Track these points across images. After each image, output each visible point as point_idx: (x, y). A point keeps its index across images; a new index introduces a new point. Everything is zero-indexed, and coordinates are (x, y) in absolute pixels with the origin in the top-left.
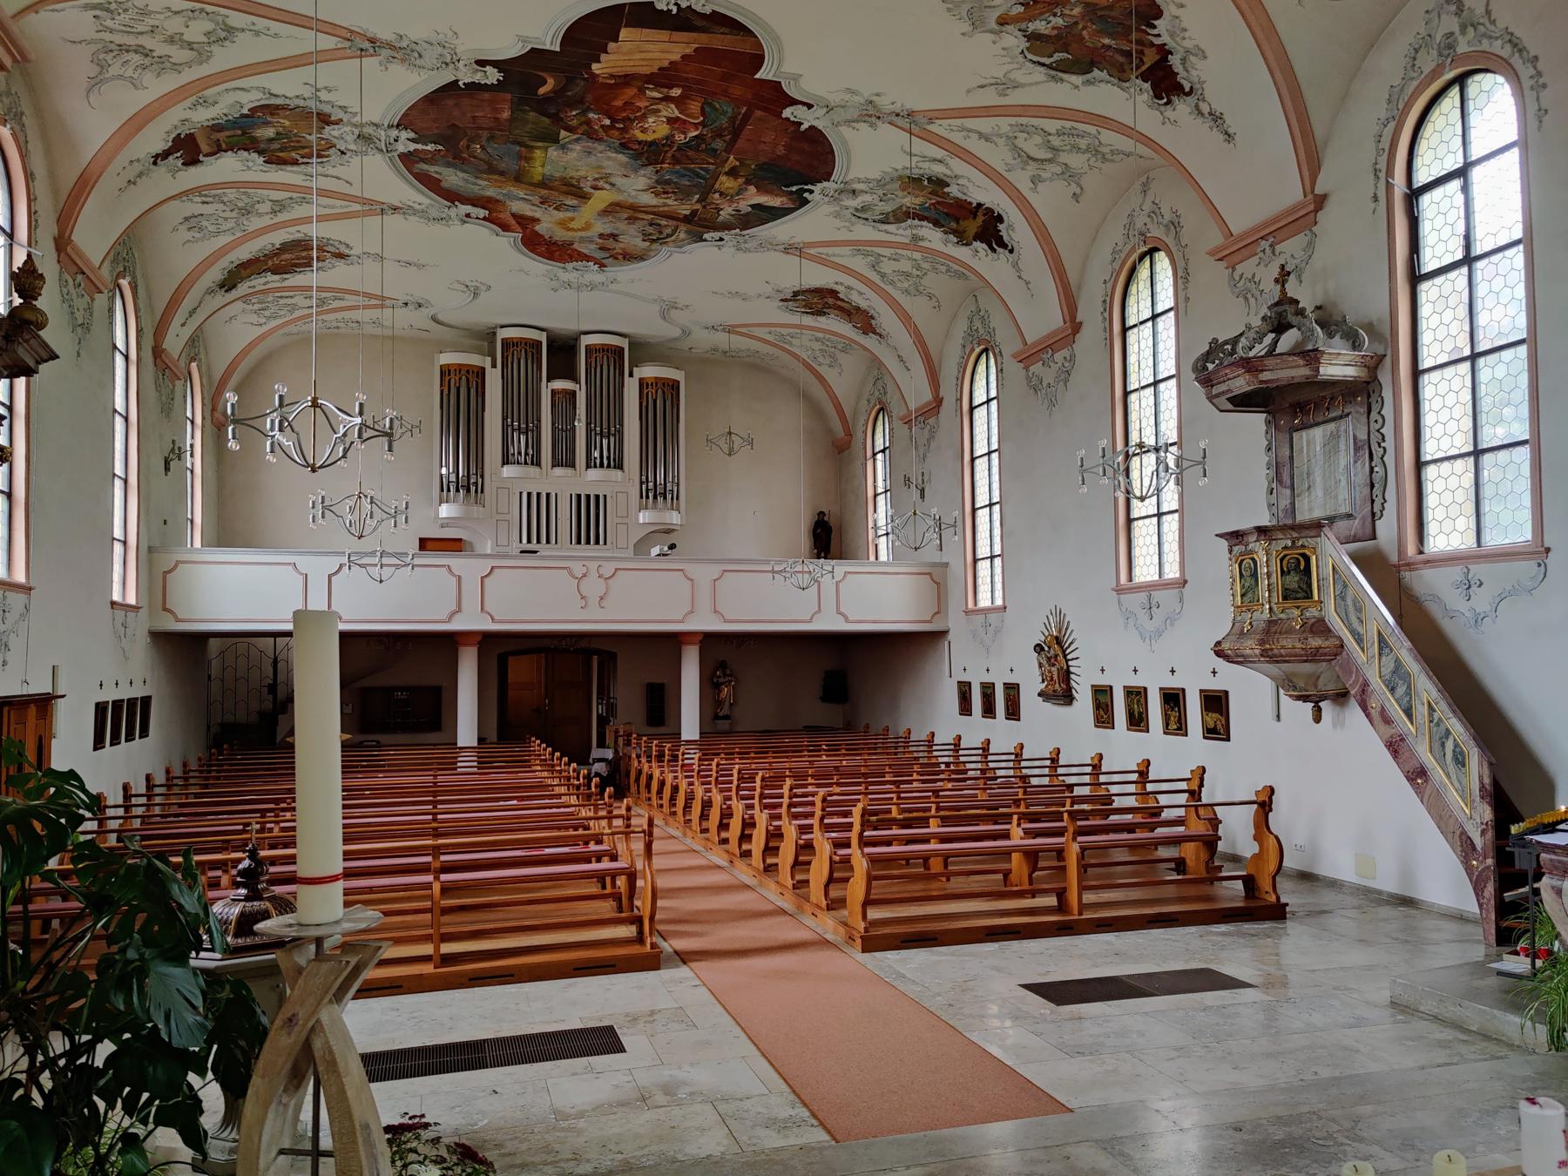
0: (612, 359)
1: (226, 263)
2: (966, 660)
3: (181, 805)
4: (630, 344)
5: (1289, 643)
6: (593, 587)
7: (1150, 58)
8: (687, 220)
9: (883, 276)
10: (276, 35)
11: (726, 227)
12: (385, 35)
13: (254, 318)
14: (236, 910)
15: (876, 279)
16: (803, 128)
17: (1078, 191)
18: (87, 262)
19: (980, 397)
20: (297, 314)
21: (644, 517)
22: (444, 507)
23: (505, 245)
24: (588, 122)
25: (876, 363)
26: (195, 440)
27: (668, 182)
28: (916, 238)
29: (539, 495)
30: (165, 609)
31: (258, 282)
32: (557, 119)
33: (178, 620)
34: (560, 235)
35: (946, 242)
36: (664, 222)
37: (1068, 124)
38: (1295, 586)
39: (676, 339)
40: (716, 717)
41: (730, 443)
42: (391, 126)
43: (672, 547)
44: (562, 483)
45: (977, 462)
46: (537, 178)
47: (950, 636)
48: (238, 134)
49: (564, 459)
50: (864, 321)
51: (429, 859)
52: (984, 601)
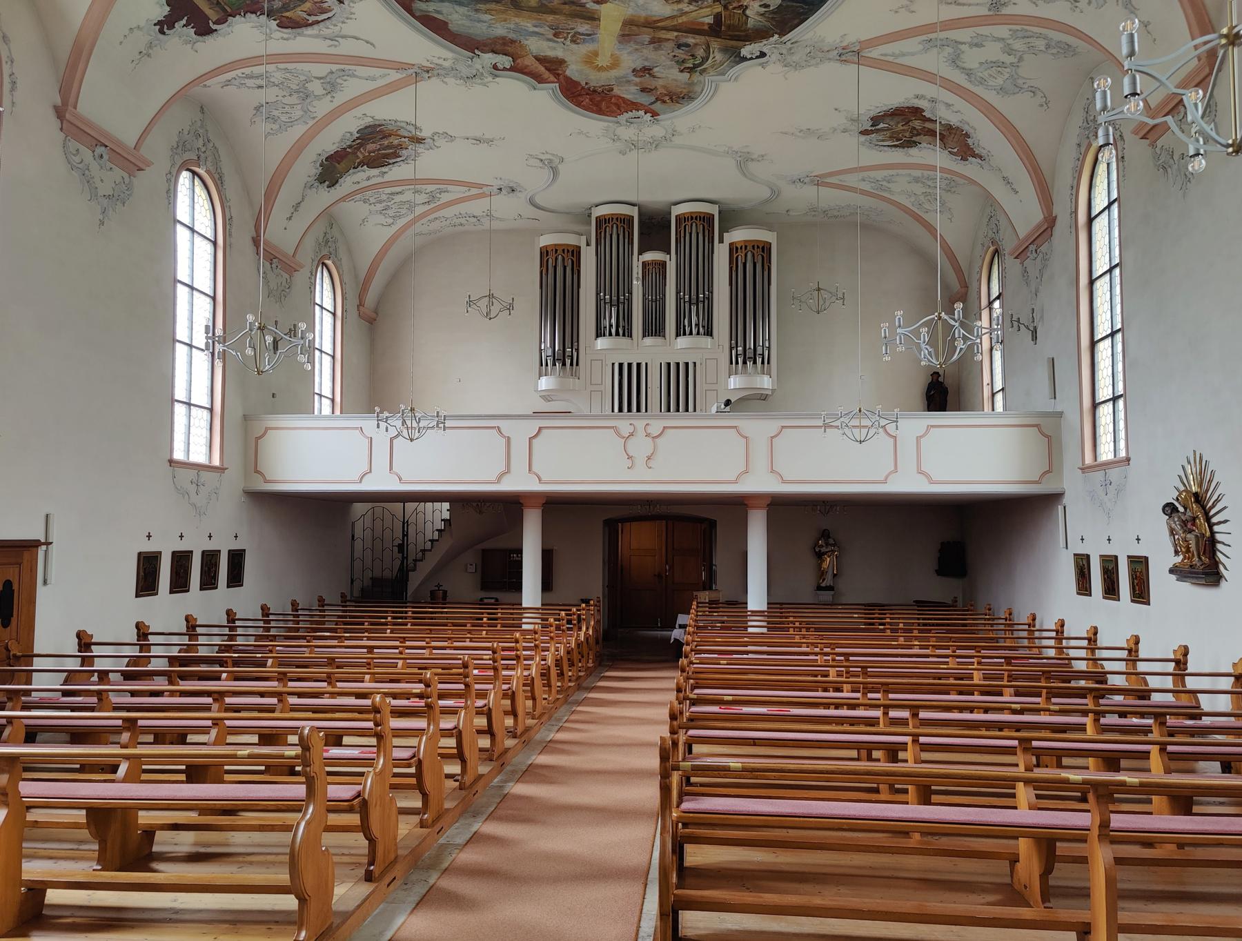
0: (703, 226)
2: (1085, 529)
4: (720, 212)
6: (640, 447)
9: (969, 73)
11: (761, 34)
19: (1100, 202)
21: (734, 382)
22: (544, 379)
23: (543, 101)
25: (989, 200)
29: (630, 365)
30: (257, 472)
33: (266, 481)
36: (691, 40)
39: (767, 201)
40: (819, 588)
44: (651, 352)
45: (1098, 284)
49: (654, 328)
50: (958, 142)
52: (1106, 453)
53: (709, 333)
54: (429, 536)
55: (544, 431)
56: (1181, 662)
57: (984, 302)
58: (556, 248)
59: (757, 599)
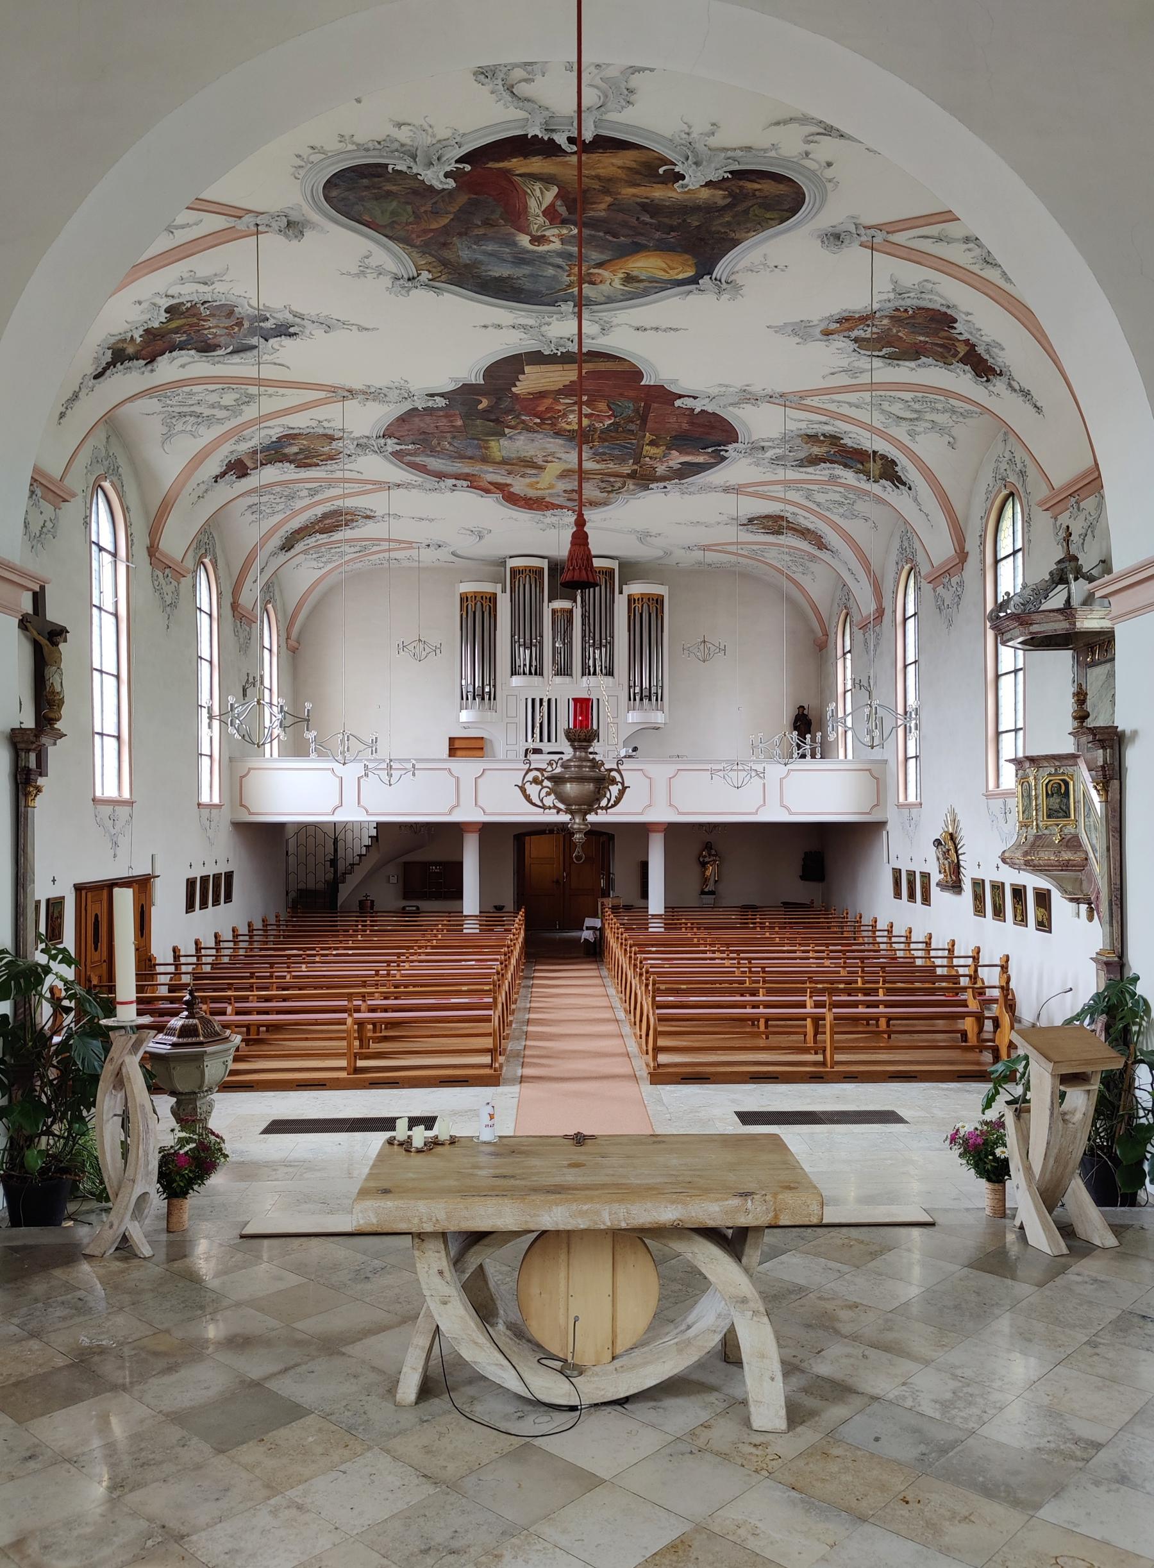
1: (283, 533)
3: (261, 949)
5: (1047, 856)
7: (962, 350)
8: (632, 475)
9: (819, 504)
10: (283, 395)
12: (357, 386)
13: (315, 564)
14: (180, 1023)
15: (814, 507)
16: (696, 411)
17: (951, 440)
18: (172, 560)
20: (347, 558)
21: (633, 717)
22: (464, 712)
24: (523, 422)
26: (270, 670)
27: (604, 454)
28: (832, 477)
30: (242, 805)
31: (311, 541)
32: (497, 421)
33: (251, 814)
34: (532, 493)
35: (859, 480)
36: (612, 479)
37: (920, 395)
38: (1057, 807)
39: (661, 558)
40: (703, 893)
41: (706, 651)
42: (378, 437)
43: (635, 749)
46: (499, 459)
47: (888, 827)
48: (274, 453)
49: (564, 670)
51: (346, 1003)
53: (610, 673)
54: (357, 851)
55: (487, 772)
56: (928, 944)
57: (840, 653)
58: (477, 596)
59: (656, 903)
